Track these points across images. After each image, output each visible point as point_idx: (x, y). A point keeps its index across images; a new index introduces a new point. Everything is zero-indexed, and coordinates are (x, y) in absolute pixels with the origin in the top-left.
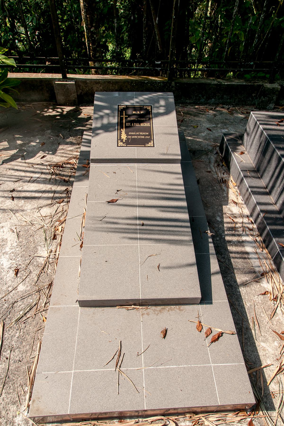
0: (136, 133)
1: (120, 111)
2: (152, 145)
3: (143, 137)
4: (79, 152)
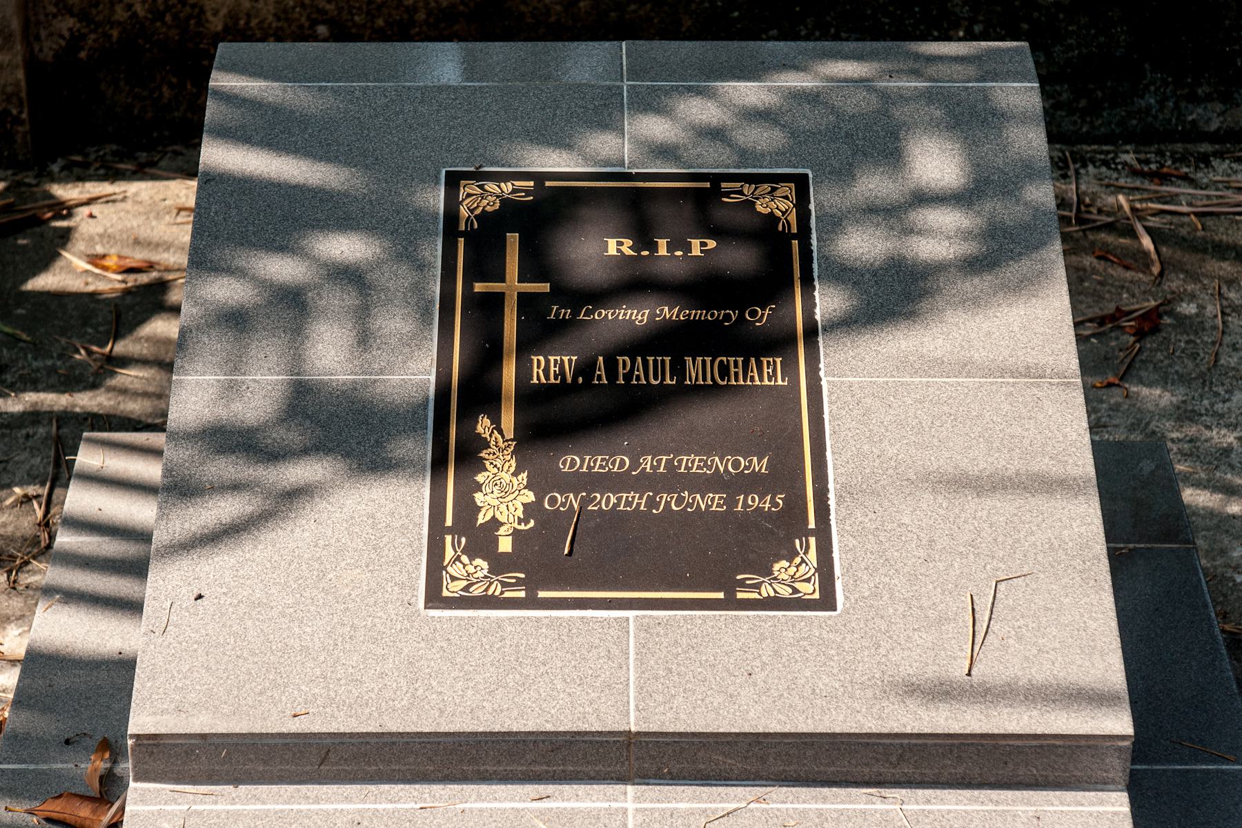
0: (635, 464)
1: (469, 235)
2: (809, 590)
3: (713, 502)
4: (13, 662)
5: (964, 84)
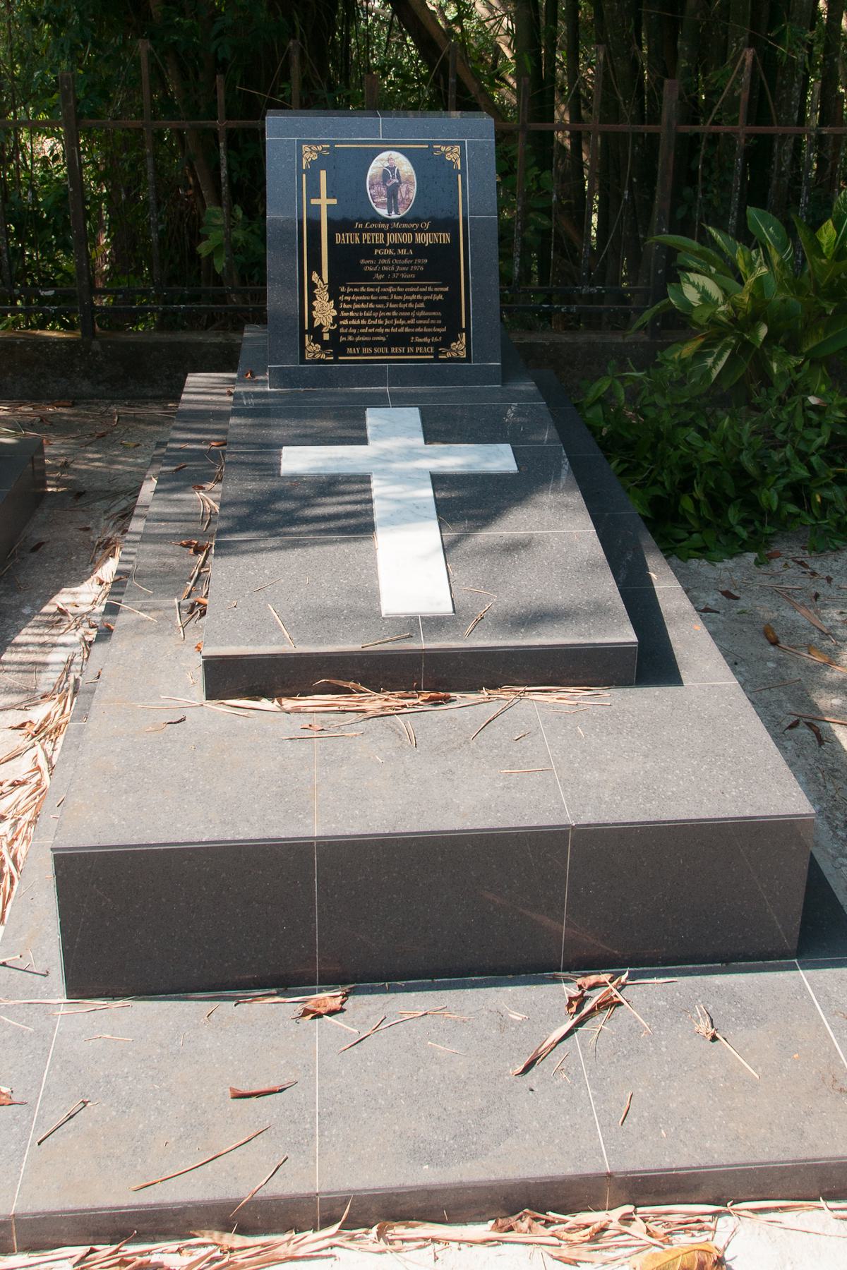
5: (736, 71)
